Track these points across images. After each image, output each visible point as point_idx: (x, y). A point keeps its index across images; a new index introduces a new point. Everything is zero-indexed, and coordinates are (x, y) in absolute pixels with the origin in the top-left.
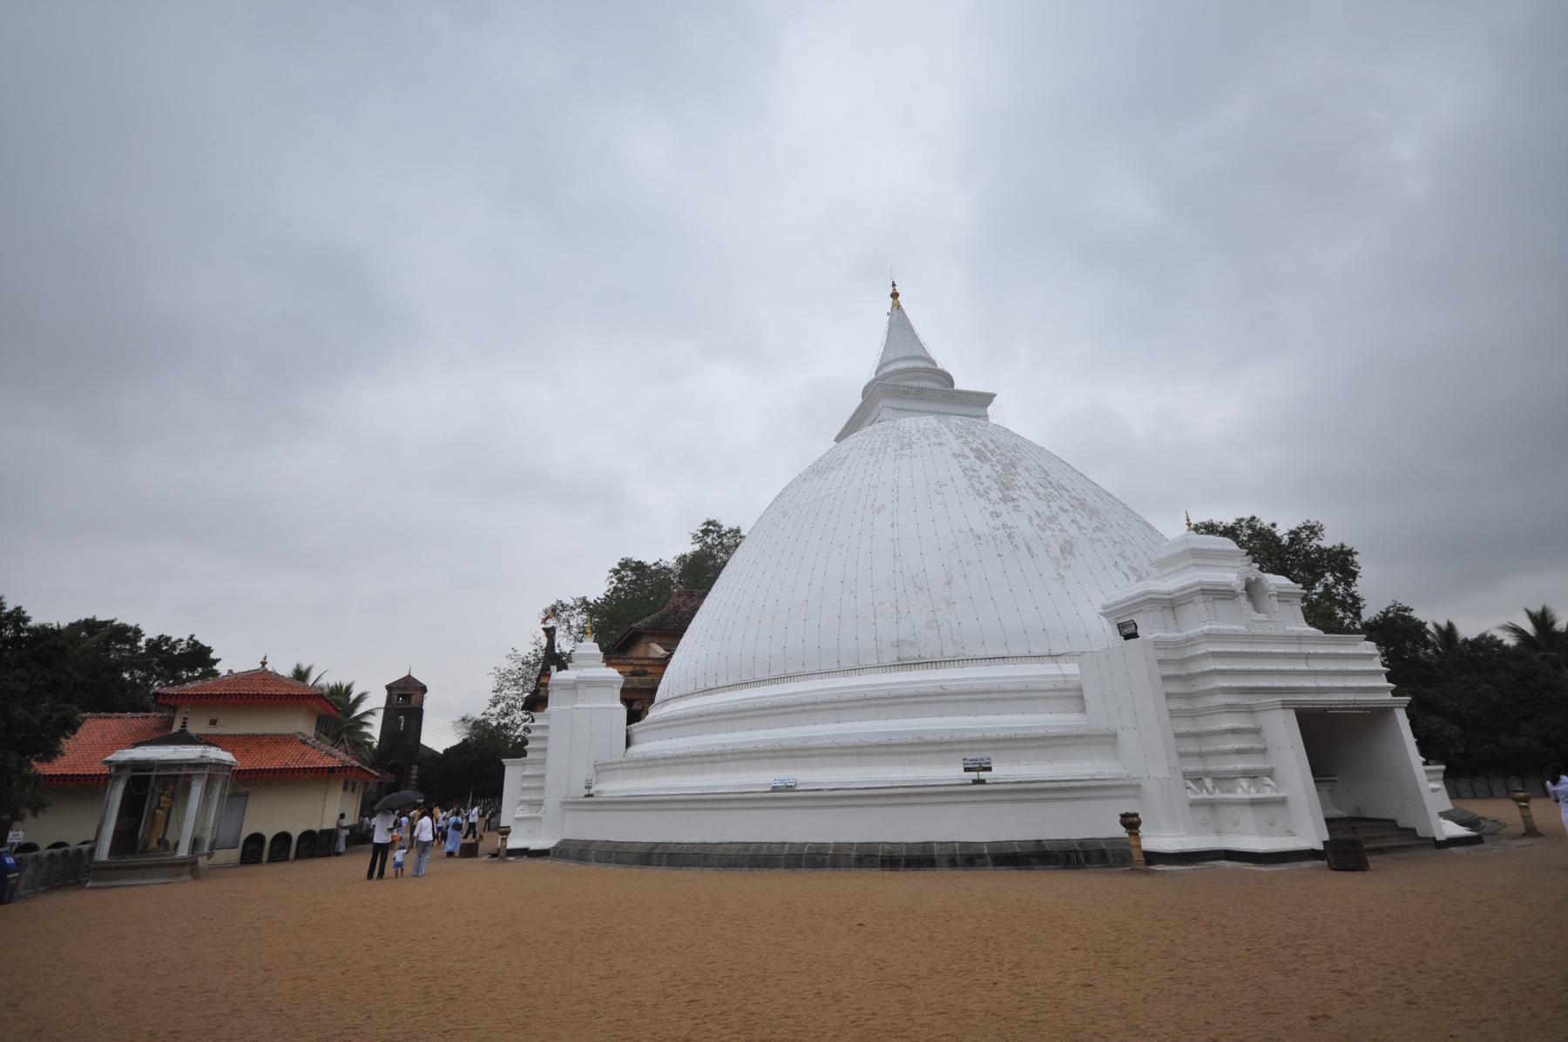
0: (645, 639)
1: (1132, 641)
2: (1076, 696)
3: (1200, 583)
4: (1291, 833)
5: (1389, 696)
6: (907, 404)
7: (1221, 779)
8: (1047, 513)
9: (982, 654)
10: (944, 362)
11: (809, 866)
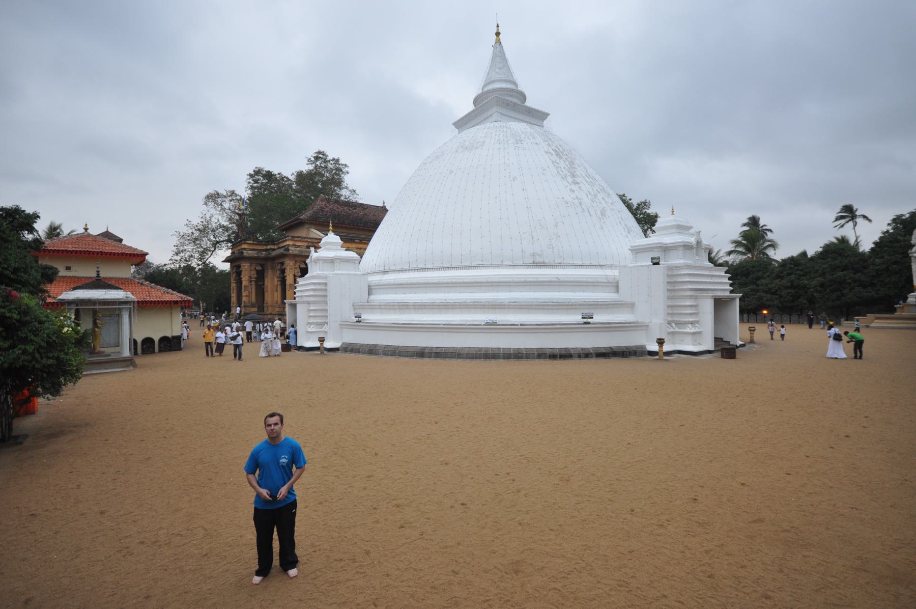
0: (307, 226)
2: (615, 286)
4: (700, 344)
5: (728, 293)
6: (512, 114)
7: (678, 323)
9: (571, 263)
10: (522, 87)
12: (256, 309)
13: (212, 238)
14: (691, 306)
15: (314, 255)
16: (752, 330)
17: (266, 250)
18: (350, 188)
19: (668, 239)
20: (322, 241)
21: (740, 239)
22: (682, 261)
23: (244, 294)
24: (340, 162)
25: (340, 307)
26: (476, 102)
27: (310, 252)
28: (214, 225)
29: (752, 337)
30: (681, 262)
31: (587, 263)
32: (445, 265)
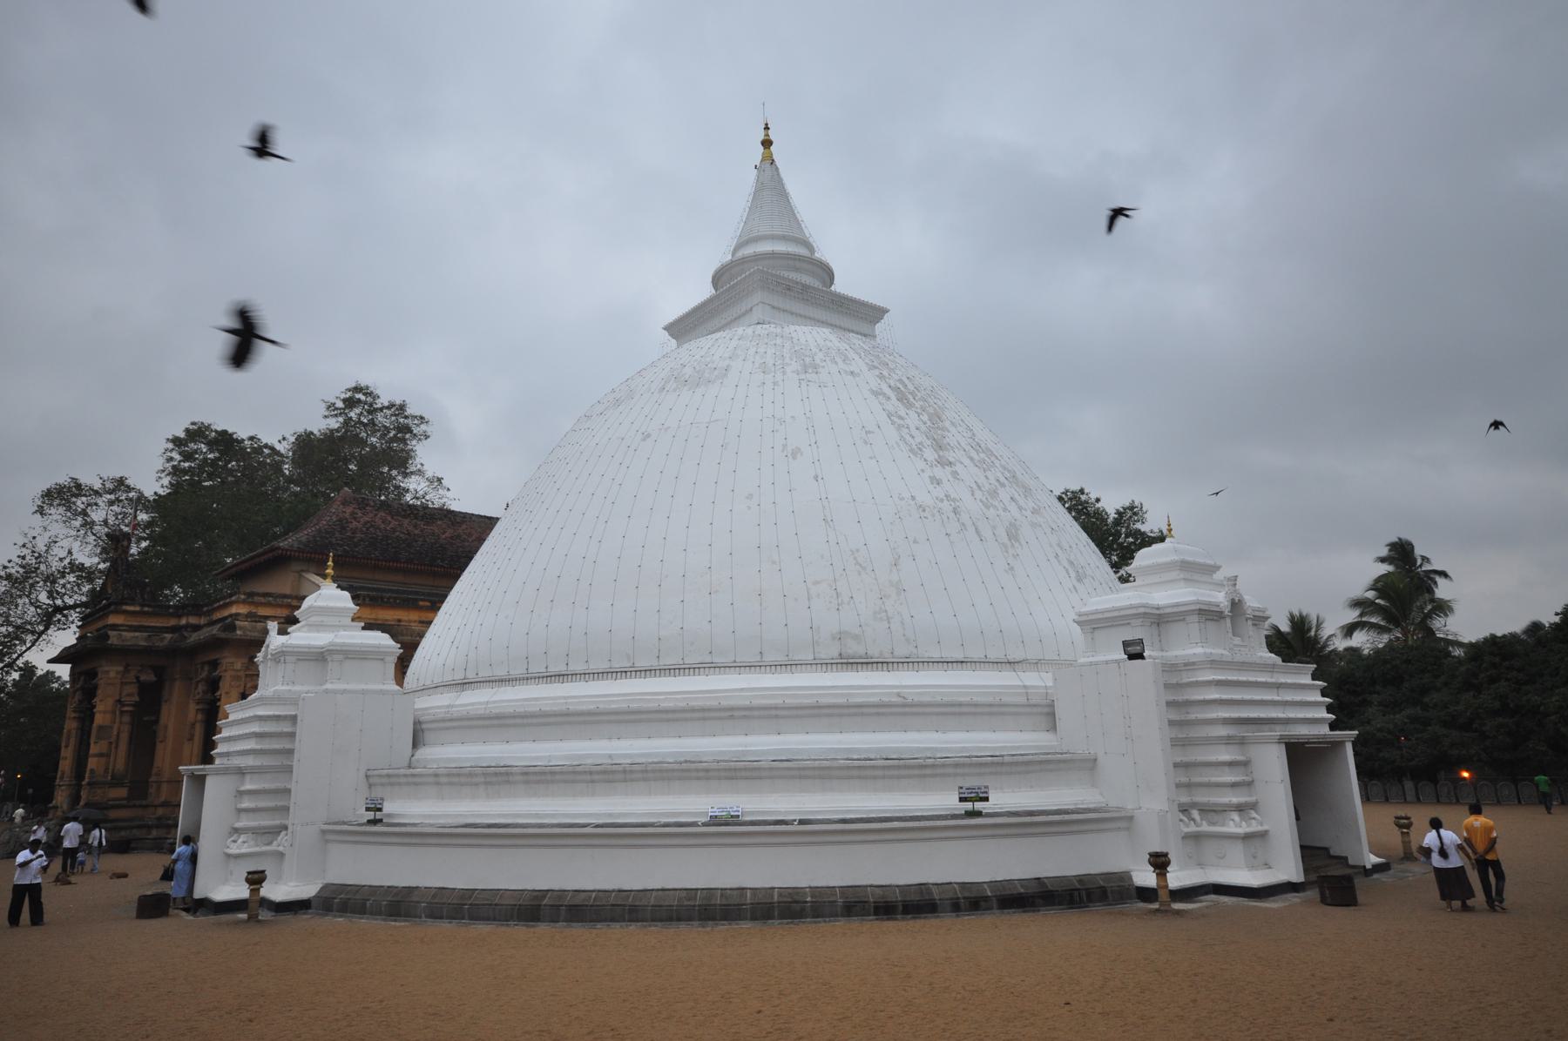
0: (296, 567)
1: (1138, 662)
3: (1198, 602)
4: (1267, 866)
5: (1325, 730)
7: (1208, 811)
8: (987, 487)
9: (936, 655)
10: (827, 251)
11: (782, 917)
12: (122, 792)
13: (43, 597)
14: (1231, 764)
15: (275, 640)
16: (1404, 825)
17: (173, 629)
18: (429, 474)
19: (1166, 596)
20: (306, 603)
21: (1371, 595)
22: (1199, 650)
23: (94, 749)
24: (409, 411)
25: (325, 785)
26: (717, 280)
27: (266, 632)
28: (56, 565)
29: (1406, 844)
30: (1196, 651)
31: (976, 654)
32: (617, 665)
